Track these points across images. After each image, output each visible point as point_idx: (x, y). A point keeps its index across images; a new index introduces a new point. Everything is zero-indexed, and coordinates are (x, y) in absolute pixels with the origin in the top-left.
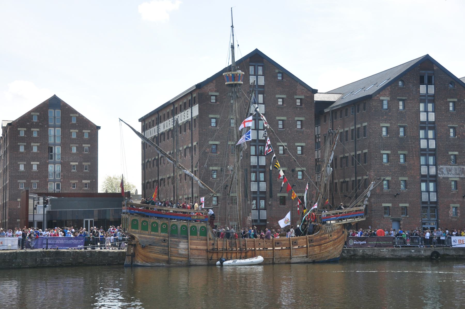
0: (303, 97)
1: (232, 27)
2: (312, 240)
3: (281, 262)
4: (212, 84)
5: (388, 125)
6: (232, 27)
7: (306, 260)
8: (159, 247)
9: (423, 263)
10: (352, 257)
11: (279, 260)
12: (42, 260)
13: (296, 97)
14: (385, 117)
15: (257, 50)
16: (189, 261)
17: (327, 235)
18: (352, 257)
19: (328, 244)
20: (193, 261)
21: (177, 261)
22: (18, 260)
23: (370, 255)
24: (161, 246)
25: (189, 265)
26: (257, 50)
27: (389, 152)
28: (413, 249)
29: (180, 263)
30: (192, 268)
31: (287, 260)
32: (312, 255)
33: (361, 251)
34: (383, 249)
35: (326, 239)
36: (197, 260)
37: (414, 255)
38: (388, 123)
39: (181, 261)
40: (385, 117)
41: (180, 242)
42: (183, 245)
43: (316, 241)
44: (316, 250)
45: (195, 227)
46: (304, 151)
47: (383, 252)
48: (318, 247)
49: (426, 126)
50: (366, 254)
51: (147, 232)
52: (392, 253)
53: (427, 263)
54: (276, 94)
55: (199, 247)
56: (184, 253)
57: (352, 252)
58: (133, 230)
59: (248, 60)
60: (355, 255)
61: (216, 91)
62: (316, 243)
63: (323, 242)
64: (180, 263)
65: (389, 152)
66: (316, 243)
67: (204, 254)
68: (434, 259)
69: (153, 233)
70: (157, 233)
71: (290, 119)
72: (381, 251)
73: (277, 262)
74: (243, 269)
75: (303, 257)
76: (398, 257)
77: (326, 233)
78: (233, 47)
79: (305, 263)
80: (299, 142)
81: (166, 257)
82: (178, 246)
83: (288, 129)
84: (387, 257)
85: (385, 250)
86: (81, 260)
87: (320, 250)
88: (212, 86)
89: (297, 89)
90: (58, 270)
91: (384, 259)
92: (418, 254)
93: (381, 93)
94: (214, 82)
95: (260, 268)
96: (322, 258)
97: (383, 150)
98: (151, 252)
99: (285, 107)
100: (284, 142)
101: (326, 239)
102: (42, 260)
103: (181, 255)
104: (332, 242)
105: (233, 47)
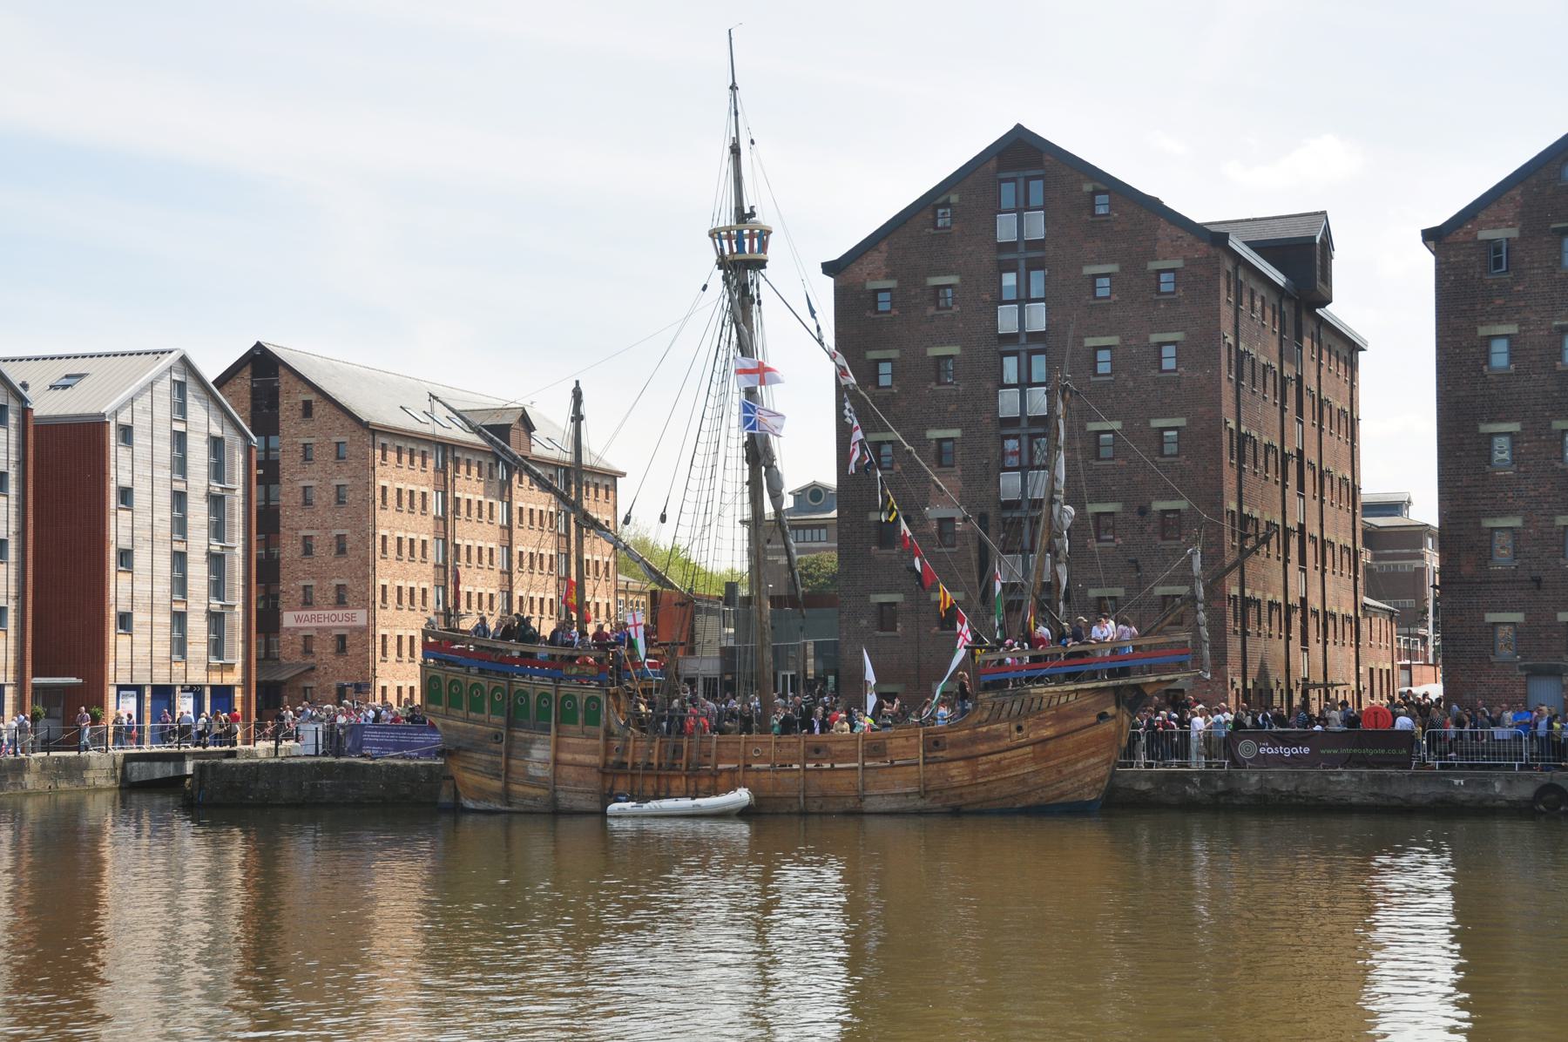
0: (1178, 263)
1: (733, 87)
2: (936, 743)
3: (831, 807)
4: (876, 254)
5: (1512, 329)
6: (733, 87)
7: (920, 804)
8: (484, 757)
9: (1500, 827)
10: (1222, 799)
11: (820, 801)
12: (314, 786)
13: (1153, 266)
14: (1499, 302)
15: (1019, 128)
16: (555, 800)
17: (1002, 726)
18: (1222, 799)
19: (1008, 754)
20: (565, 801)
21: (525, 796)
22: (261, 785)
23: (1289, 795)
24: (489, 752)
25: (556, 813)
26: (1019, 128)
27: (1514, 427)
28: (1458, 776)
29: (531, 803)
30: (563, 823)
31: (850, 804)
32: (940, 790)
33: (1254, 779)
34: (1340, 774)
35: (1000, 737)
36: (572, 796)
37: (1462, 797)
38: (1509, 321)
39: (535, 799)
40: (1499, 302)
41: (532, 742)
42: (540, 753)
43: (954, 745)
44: (954, 772)
45: (573, 698)
46: (1156, 445)
47: (1339, 783)
48: (961, 763)
49: (1024, 344)
50: (1275, 791)
51: (460, 713)
52: (1376, 789)
53: (1525, 829)
54: (1085, 263)
55: (580, 758)
56: (540, 774)
57: (1220, 783)
58: (432, 707)
59: (993, 164)
60: (1229, 793)
61: (887, 277)
62: (957, 753)
63: (984, 748)
64: (531, 803)
65: (1514, 427)
66: (957, 753)
67: (594, 778)
68: (1542, 813)
69: (472, 715)
70: (480, 717)
71: (1133, 342)
72: (1330, 782)
73: (815, 810)
74: (664, 826)
75: (907, 794)
76: (1395, 802)
77: (998, 721)
78: (735, 150)
79: (919, 813)
80: (1165, 416)
81: (497, 785)
82: (528, 754)
83: (1124, 375)
84: (1354, 800)
85: (1345, 777)
86: (406, 791)
87: (974, 775)
88: (877, 259)
89: (1157, 240)
90: (1251, 828)
91: (1343, 809)
92: (1481, 792)
93: (1482, 216)
94: (884, 246)
95: (742, 830)
96: (1062, 795)
97: (1491, 421)
98: (465, 769)
99: (1115, 303)
100: (1111, 418)
101: (1000, 737)
102: (314, 786)
103: (534, 781)
104: (1028, 749)
105: (735, 150)
